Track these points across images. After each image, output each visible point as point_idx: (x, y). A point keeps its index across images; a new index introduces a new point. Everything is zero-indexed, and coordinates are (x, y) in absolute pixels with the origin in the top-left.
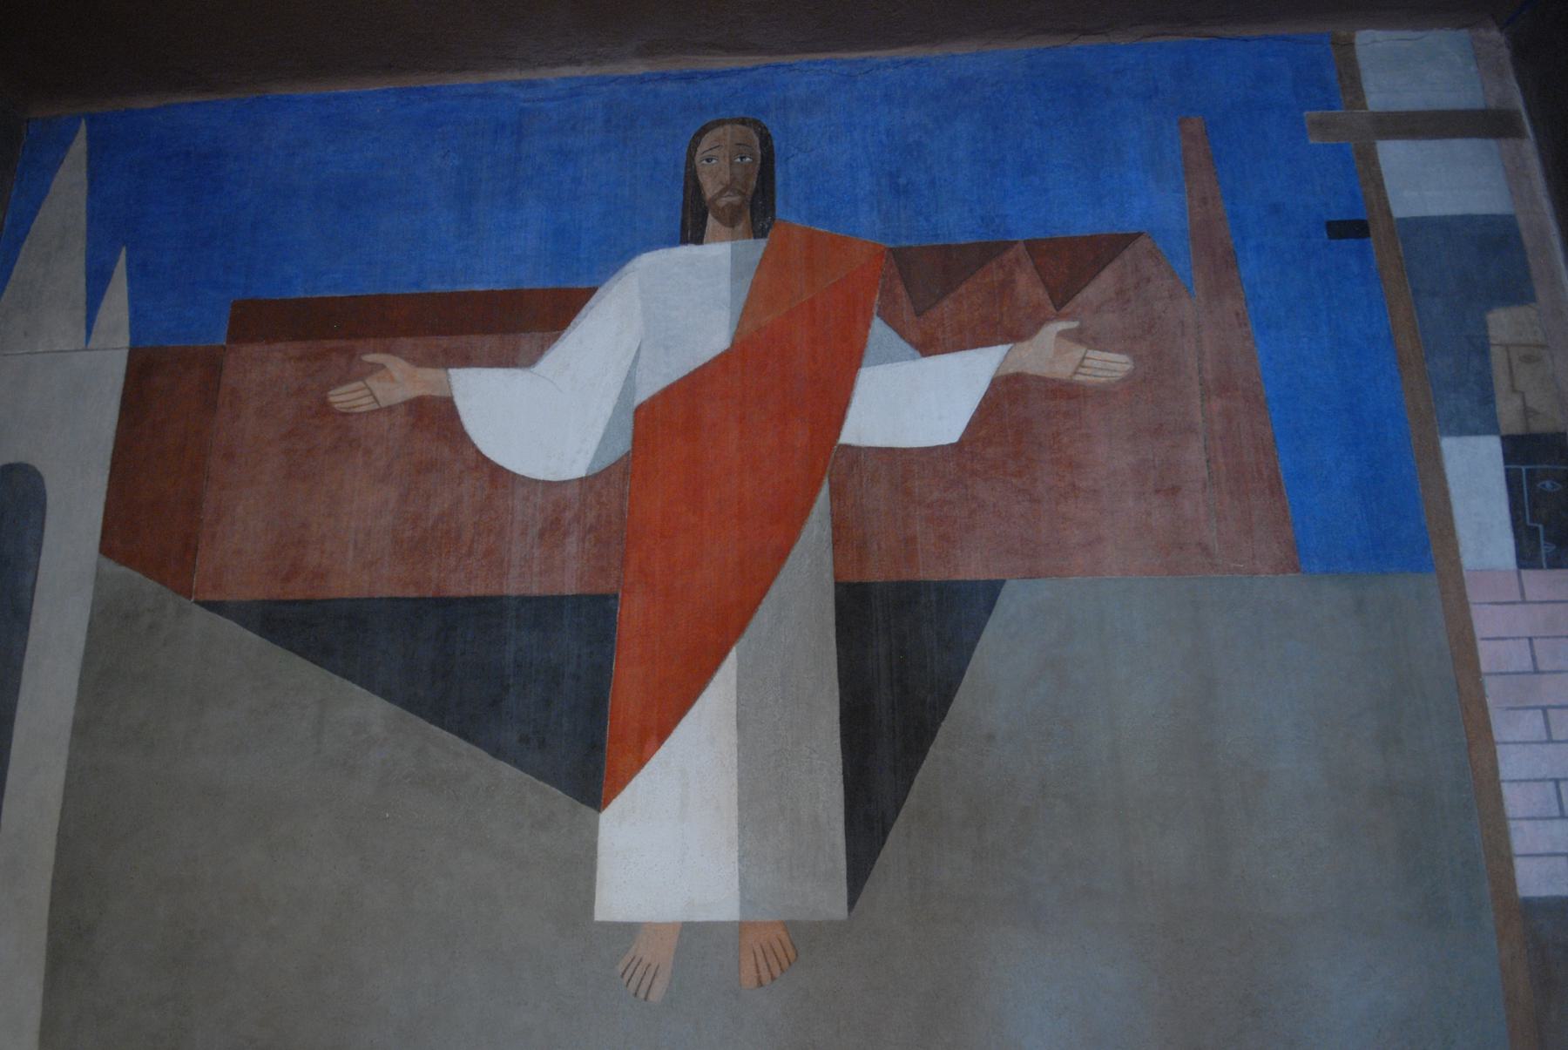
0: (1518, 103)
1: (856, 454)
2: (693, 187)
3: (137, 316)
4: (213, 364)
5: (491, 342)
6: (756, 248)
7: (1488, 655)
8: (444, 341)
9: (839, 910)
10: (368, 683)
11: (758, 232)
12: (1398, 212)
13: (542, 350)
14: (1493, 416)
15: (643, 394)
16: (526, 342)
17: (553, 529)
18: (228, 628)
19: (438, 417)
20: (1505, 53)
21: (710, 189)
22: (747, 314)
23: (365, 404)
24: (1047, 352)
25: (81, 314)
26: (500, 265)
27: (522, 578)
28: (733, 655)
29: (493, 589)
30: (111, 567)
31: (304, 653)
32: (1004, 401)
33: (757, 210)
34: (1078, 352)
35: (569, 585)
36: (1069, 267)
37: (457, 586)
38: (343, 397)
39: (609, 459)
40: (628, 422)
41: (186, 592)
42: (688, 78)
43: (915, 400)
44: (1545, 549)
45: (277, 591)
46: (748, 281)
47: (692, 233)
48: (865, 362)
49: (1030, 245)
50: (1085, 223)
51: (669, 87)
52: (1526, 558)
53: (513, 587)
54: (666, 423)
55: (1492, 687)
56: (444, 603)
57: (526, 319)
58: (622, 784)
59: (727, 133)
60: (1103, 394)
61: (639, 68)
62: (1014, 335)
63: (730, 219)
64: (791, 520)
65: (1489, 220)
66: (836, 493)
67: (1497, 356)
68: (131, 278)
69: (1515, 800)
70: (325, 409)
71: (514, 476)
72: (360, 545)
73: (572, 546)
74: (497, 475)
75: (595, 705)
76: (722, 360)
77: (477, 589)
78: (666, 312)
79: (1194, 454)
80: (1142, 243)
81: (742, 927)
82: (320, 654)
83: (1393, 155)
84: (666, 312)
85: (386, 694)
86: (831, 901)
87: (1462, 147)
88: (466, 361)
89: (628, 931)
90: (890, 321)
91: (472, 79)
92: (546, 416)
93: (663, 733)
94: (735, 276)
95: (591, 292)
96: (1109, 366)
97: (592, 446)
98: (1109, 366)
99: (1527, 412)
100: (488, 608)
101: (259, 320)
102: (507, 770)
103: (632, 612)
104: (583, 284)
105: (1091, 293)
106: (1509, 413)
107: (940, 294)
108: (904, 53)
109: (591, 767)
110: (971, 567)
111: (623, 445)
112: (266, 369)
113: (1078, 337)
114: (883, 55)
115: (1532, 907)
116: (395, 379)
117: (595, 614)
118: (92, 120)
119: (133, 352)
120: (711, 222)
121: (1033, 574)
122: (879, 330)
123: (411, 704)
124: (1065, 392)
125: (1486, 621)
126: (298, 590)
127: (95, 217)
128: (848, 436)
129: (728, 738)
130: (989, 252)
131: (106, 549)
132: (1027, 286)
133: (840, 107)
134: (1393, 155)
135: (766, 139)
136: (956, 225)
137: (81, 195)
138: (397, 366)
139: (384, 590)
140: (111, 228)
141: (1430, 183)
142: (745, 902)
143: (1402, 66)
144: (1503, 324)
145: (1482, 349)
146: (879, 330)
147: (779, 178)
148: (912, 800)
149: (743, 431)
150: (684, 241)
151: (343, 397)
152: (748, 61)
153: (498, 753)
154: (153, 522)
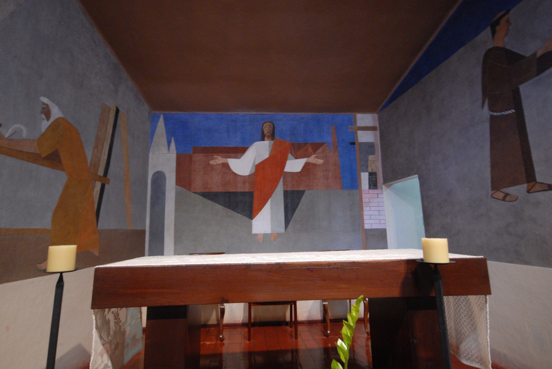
0: (378, 126)
1: (286, 173)
2: (263, 132)
3: (177, 149)
4: (191, 157)
5: (233, 155)
6: (272, 142)
7: (364, 200)
8: (227, 154)
9: (284, 232)
10: (219, 203)
11: (273, 140)
12: (359, 141)
13: (241, 156)
14: (243, 194)
15: (256, 163)
16: (239, 155)
17: (244, 182)
18: (197, 196)
19: (226, 166)
20: (377, 118)
21: (265, 133)
22: (271, 152)
23: (215, 164)
24: (312, 159)
25: (167, 147)
26: (235, 143)
27: (240, 189)
28: (270, 200)
29: (236, 191)
30: (178, 187)
31: (209, 199)
32: (307, 165)
33: (272, 136)
34: (316, 159)
35: (247, 190)
36: (316, 147)
37: (231, 190)
38: (211, 162)
39: (252, 172)
40: (254, 167)
41: (190, 191)
42: (262, 115)
43: (294, 165)
44: (372, 187)
45: (204, 191)
46: (271, 147)
47: (263, 139)
48: (288, 158)
49: (311, 143)
50: (318, 141)
51: (258, 116)
52: (370, 188)
53: (239, 190)
54: (260, 167)
55: (364, 204)
56: (229, 193)
57: (239, 151)
58: (255, 217)
59: (268, 124)
60: (319, 165)
61: (255, 113)
62: (308, 156)
63: (268, 137)
64: (277, 182)
65: (371, 143)
66: (284, 178)
67: (369, 162)
68: (175, 142)
69: (365, 217)
70: (209, 164)
71: (238, 175)
72: (216, 186)
73: (247, 185)
74: (235, 174)
75: (251, 206)
76: (268, 159)
77: (234, 191)
78: (259, 151)
79: (331, 174)
80: (326, 144)
81: (271, 234)
82: (212, 199)
83: (360, 133)
84: (259, 151)
85: (222, 205)
86: (282, 230)
87: (369, 132)
88: (230, 157)
89: (257, 235)
90: (292, 154)
91: (229, 113)
92: (243, 166)
93: (261, 209)
94: (269, 146)
95: (248, 148)
96: (320, 161)
97: (249, 170)
98: (320, 161)
99: (372, 169)
100: (235, 193)
101: (197, 150)
102: (239, 215)
103: (256, 194)
104: (247, 146)
105: (319, 151)
106: (370, 170)
107: (299, 151)
108: (293, 113)
109: (251, 214)
110: (301, 189)
111: (254, 171)
112: (199, 158)
113: (317, 157)
114: (291, 113)
115: (366, 230)
116: (219, 160)
117: (251, 194)
118: (164, 114)
119: (177, 154)
120: (266, 138)
121: (309, 190)
122: (290, 155)
123: (225, 206)
124: (315, 165)
125: (364, 196)
126: (207, 191)
127: (167, 132)
128: (286, 170)
129: (269, 210)
130: (305, 144)
131: (177, 184)
132: (310, 150)
133: (285, 120)
134: (360, 133)
135: (274, 125)
136: (301, 140)
137: (163, 127)
138: (219, 158)
139: (220, 191)
140: (171, 133)
141: (364, 137)
142: (272, 231)
143: (365, 119)
144: (371, 157)
145: (367, 161)
146: (290, 155)
147: (275, 131)
148: (293, 218)
149: (269, 170)
150: (262, 140)
151: (211, 162)
152: (271, 113)
153: (238, 212)
154: (184, 179)
